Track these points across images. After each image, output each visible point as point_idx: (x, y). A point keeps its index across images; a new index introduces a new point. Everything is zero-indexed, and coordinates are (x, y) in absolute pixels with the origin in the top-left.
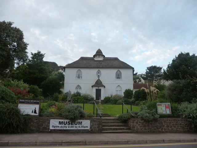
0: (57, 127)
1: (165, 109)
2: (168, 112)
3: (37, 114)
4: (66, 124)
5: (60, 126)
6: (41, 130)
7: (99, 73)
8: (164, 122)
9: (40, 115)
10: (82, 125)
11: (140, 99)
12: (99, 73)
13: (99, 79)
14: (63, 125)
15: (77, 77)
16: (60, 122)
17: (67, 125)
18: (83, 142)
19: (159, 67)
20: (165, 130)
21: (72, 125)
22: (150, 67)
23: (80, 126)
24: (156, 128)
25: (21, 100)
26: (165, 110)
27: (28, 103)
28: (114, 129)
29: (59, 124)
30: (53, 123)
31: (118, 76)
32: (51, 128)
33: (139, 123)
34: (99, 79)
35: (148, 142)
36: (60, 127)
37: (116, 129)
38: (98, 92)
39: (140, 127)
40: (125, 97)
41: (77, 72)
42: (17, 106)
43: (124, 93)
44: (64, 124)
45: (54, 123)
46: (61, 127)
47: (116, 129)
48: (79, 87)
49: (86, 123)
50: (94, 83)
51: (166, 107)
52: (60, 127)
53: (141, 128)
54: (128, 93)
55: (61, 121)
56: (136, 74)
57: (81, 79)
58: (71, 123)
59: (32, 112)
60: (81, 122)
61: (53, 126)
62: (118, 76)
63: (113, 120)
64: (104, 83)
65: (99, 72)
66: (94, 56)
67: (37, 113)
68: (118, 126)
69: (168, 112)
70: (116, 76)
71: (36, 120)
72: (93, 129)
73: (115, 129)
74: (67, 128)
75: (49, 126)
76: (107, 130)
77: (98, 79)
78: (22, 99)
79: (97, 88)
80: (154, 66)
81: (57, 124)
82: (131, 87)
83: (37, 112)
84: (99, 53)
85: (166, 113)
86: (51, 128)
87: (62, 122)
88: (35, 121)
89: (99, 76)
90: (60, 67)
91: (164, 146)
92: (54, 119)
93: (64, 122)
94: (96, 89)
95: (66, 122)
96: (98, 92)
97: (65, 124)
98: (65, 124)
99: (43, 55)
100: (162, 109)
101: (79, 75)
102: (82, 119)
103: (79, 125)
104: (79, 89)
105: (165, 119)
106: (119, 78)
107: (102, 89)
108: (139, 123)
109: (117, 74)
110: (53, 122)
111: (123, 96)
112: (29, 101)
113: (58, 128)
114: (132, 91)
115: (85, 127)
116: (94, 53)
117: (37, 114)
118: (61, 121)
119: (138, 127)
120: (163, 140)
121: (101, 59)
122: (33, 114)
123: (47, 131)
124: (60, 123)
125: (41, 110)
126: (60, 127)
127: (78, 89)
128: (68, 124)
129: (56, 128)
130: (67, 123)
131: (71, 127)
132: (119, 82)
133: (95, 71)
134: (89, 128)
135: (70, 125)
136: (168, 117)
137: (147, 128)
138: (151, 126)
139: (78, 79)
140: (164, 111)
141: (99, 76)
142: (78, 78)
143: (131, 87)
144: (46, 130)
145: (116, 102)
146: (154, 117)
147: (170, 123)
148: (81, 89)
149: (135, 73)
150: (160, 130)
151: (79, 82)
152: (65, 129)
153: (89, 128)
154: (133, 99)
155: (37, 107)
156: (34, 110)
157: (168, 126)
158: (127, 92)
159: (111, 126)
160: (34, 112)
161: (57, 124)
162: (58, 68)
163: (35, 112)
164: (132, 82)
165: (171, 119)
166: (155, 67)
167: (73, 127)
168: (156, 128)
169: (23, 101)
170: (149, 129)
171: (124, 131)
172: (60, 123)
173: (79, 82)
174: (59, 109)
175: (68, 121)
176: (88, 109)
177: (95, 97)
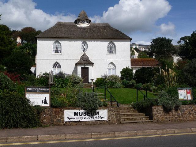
0: (72, 118)
2: (190, 98)
3: (48, 105)
5: (75, 117)
6: (55, 123)
8: (186, 110)
9: (52, 105)
12: (84, 45)
13: (84, 55)
14: (79, 116)
15: (54, 52)
17: (83, 116)
20: (186, 118)
23: (97, 116)
24: (177, 116)
25: (28, 89)
26: (186, 96)
28: (132, 119)
30: (68, 114)
31: (111, 51)
32: (66, 120)
33: (159, 112)
34: (84, 55)
36: (75, 118)
37: (135, 119)
38: (85, 71)
39: (161, 116)
40: (122, 78)
41: (109, 44)
43: (121, 72)
44: (80, 115)
45: (69, 115)
46: (77, 118)
48: (57, 65)
49: (104, 113)
50: (77, 60)
51: (187, 93)
52: (76, 119)
53: (162, 117)
54: (126, 72)
55: (76, 111)
57: (59, 53)
58: (87, 113)
59: (42, 102)
60: (98, 112)
61: (68, 118)
62: (111, 51)
64: (91, 59)
66: (77, 22)
67: (47, 104)
68: (135, 115)
69: (190, 98)
70: (108, 49)
71: (49, 111)
72: (110, 119)
73: (133, 119)
74: (83, 120)
76: (124, 120)
78: (29, 87)
82: (128, 65)
83: (48, 102)
85: (187, 98)
86: (66, 120)
87: (78, 113)
88: (48, 113)
90: (14, 32)
91: (150, 137)
92: (69, 109)
93: (80, 113)
94: (82, 68)
95: (82, 112)
97: (81, 115)
98: (81, 115)
101: (57, 48)
105: (187, 106)
106: (112, 53)
107: (90, 68)
108: (159, 112)
109: (110, 47)
110: (67, 112)
112: (38, 89)
115: (102, 118)
117: (48, 105)
118: (76, 111)
119: (158, 116)
121: (85, 25)
122: (44, 105)
126: (75, 118)
127: (55, 67)
128: (84, 115)
129: (71, 120)
130: (83, 114)
132: (112, 57)
133: (78, 44)
134: (106, 119)
135: (86, 116)
136: (190, 104)
138: (172, 114)
141: (84, 49)
143: (128, 65)
145: (113, 84)
146: (176, 104)
147: (192, 110)
148: (60, 67)
150: (182, 118)
151: (57, 58)
152: (81, 120)
153: (106, 119)
155: (47, 96)
156: (44, 100)
157: (190, 114)
159: (128, 115)
160: (44, 102)
161: (72, 115)
162: (15, 37)
163: (46, 102)
165: (193, 106)
168: (177, 116)
169: (31, 89)
170: (170, 118)
173: (57, 58)
175: (83, 111)
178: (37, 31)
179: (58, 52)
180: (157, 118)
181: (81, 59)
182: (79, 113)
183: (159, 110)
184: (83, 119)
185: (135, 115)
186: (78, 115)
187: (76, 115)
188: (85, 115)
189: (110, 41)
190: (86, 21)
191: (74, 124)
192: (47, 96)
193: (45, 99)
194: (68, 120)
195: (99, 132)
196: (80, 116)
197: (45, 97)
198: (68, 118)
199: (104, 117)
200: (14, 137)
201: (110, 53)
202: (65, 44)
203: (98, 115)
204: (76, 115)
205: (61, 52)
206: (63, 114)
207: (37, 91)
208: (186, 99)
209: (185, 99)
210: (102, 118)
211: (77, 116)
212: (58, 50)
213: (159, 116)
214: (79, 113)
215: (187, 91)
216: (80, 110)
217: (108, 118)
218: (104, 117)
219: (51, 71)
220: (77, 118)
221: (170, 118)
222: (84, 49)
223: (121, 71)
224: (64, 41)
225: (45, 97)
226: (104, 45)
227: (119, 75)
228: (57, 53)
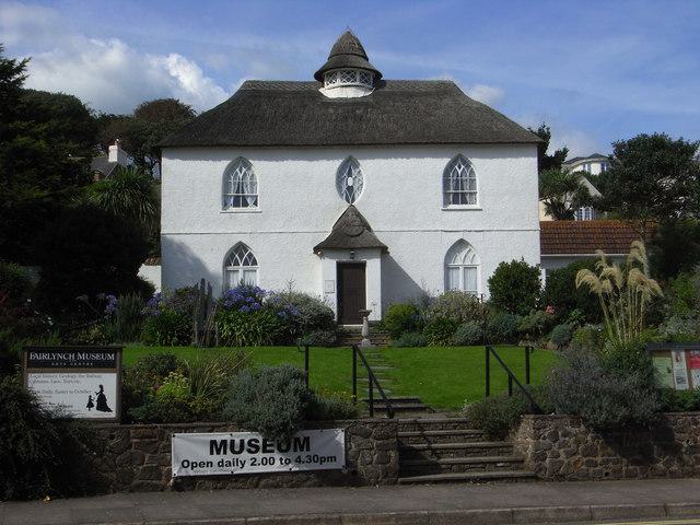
0: (201, 464)
1: (685, 371)
3: (113, 415)
4: (240, 452)
5: (216, 458)
7: (350, 174)
9: (125, 417)
10: (311, 453)
11: (575, 313)
14: (229, 456)
16: (213, 443)
17: (245, 456)
18: (331, 520)
19: (680, 143)
21: (268, 455)
22: (633, 144)
23: (304, 455)
27: (66, 367)
29: (212, 453)
31: (457, 191)
35: (598, 514)
36: (215, 464)
39: (570, 454)
41: (229, 172)
42: (23, 381)
43: (491, 281)
45: (190, 450)
46: (221, 464)
47: (462, 467)
48: (239, 254)
50: (326, 231)
54: (511, 280)
55: (219, 437)
56: (561, 155)
58: (260, 444)
59: (90, 405)
60: (307, 439)
61: (185, 464)
62: (457, 191)
63: (444, 425)
65: (347, 169)
66: (321, 76)
67: (109, 410)
74: (248, 469)
75: (169, 463)
77: (345, 206)
79: (345, 258)
80: (650, 134)
81: (203, 454)
82: (529, 253)
83: (112, 402)
84: (347, 60)
86: (176, 471)
87: (224, 442)
89: (350, 189)
92: (186, 430)
93: (233, 442)
94: (341, 267)
95: (242, 441)
96: (350, 281)
97: (237, 450)
98: (237, 450)
99: (19, 70)
100: (669, 372)
102: (308, 427)
103: (299, 453)
104: (246, 263)
106: (464, 202)
108: (562, 439)
111: (488, 296)
113: (208, 471)
114: (535, 272)
115: (323, 460)
116: (321, 61)
117: (113, 415)
118: (219, 437)
120: (664, 507)
122: (95, 413)
123: (163, 482)
124: (215, 447)
125: (125, 395)
126: (215, 464)
127: (237, 264)
128: (249, 451)
131: (265, 462)
132: (459, 220)
133: (327, 167)
134: (340, 463)
135: (260, 456)
137: (599, 459)
139: (235, 209)
140: (680, 380)
142: (236, 204)
143: (529, 253)
144: (155, 480)
148: (255, 263)
149: (550, 152)
153: (340, 463)
154: (536, 317)
155: (109, 382)
158: (508, 277)
160: (95, 403)
161: (203, 454)
163: (102, 405)
164: (538, 213)
166: (658, 143)
167: (271, 461)
169: (45, 356)
170: (610, 464)
171: (498, 473)
172: (215, 447)
173: (240, 225)
174: (196, 380)
176: (328, 373)
177: (335, 311)
178: (98, 115)
179: (245, 204)
180: (552, 463)
181: (336, 230)
182: (229, 443)
183: (560, 433)
184: (278, 462)
185: (481, 450)
186: (225, 453)
187: (218, 453)
188: (253, 449)
189: (456, 153)
190: (358, 77)
191: (304, 477)
192: (109, 382)
193: (102, 391)
194: (184, 473)
195: (504, 507)
196: (236, 456)
197: (101, 387)
198: (186, 464)
199: (333, 459)
200: (254, 519)
201: (455, 202)
202: (268, 172)
203: (308, 450)
204: (218, 453)
205: (256, 204)
206: (168, 449)
207: (68, 362)
208: (684, 386)
209: (679, 387)
210: (323, 460)
211: (222, 456)
212: (463, 194)
213: (563, 457)
214: (229, 443)
215: (689, 358)
216: (234, 434)
217: (348, 464)
218: (333, 459)
219: (203, 281)
220: (221, 464)
221: (610, 464)
222: (350, 189)
223: (492, 274)
224: (190, 159)
225: (101, 387)
226: (432, 167)
227: (483, 292)
228: (241, 209)
